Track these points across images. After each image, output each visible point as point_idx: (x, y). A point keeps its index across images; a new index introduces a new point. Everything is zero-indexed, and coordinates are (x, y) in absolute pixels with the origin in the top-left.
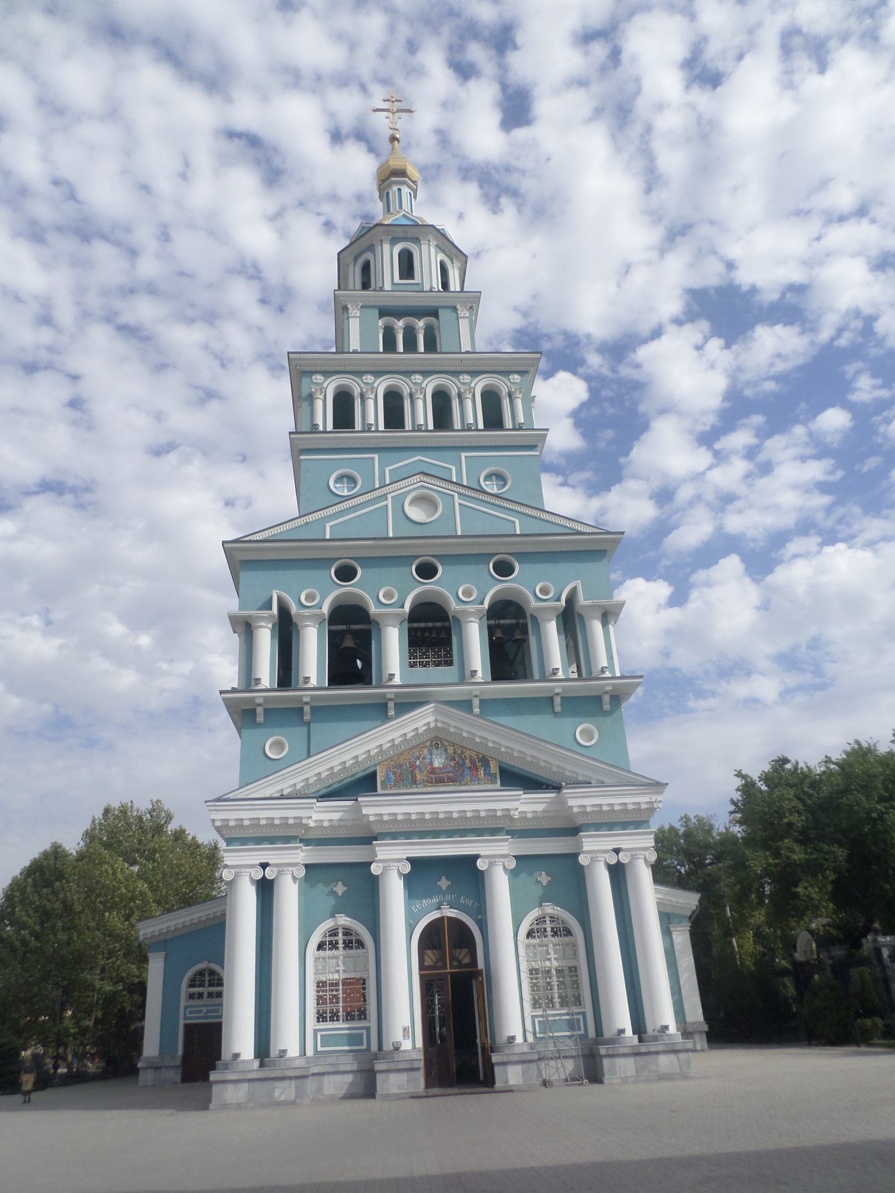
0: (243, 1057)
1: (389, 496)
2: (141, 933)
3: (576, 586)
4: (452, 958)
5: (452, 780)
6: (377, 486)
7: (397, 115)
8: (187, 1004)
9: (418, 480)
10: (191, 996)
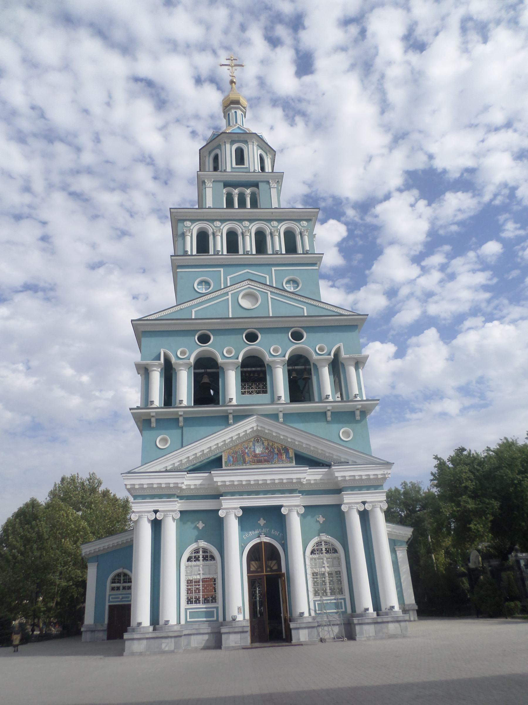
0: (144, 625)
1: (230, 293)
2: (83, 551)
3: (340, 347)
4: (267, 566)
5: (267, 461)
6: (222, 287)
7: (234, 68)
8: (111, 593)
9: (247, 283)
10: (113, 589)
